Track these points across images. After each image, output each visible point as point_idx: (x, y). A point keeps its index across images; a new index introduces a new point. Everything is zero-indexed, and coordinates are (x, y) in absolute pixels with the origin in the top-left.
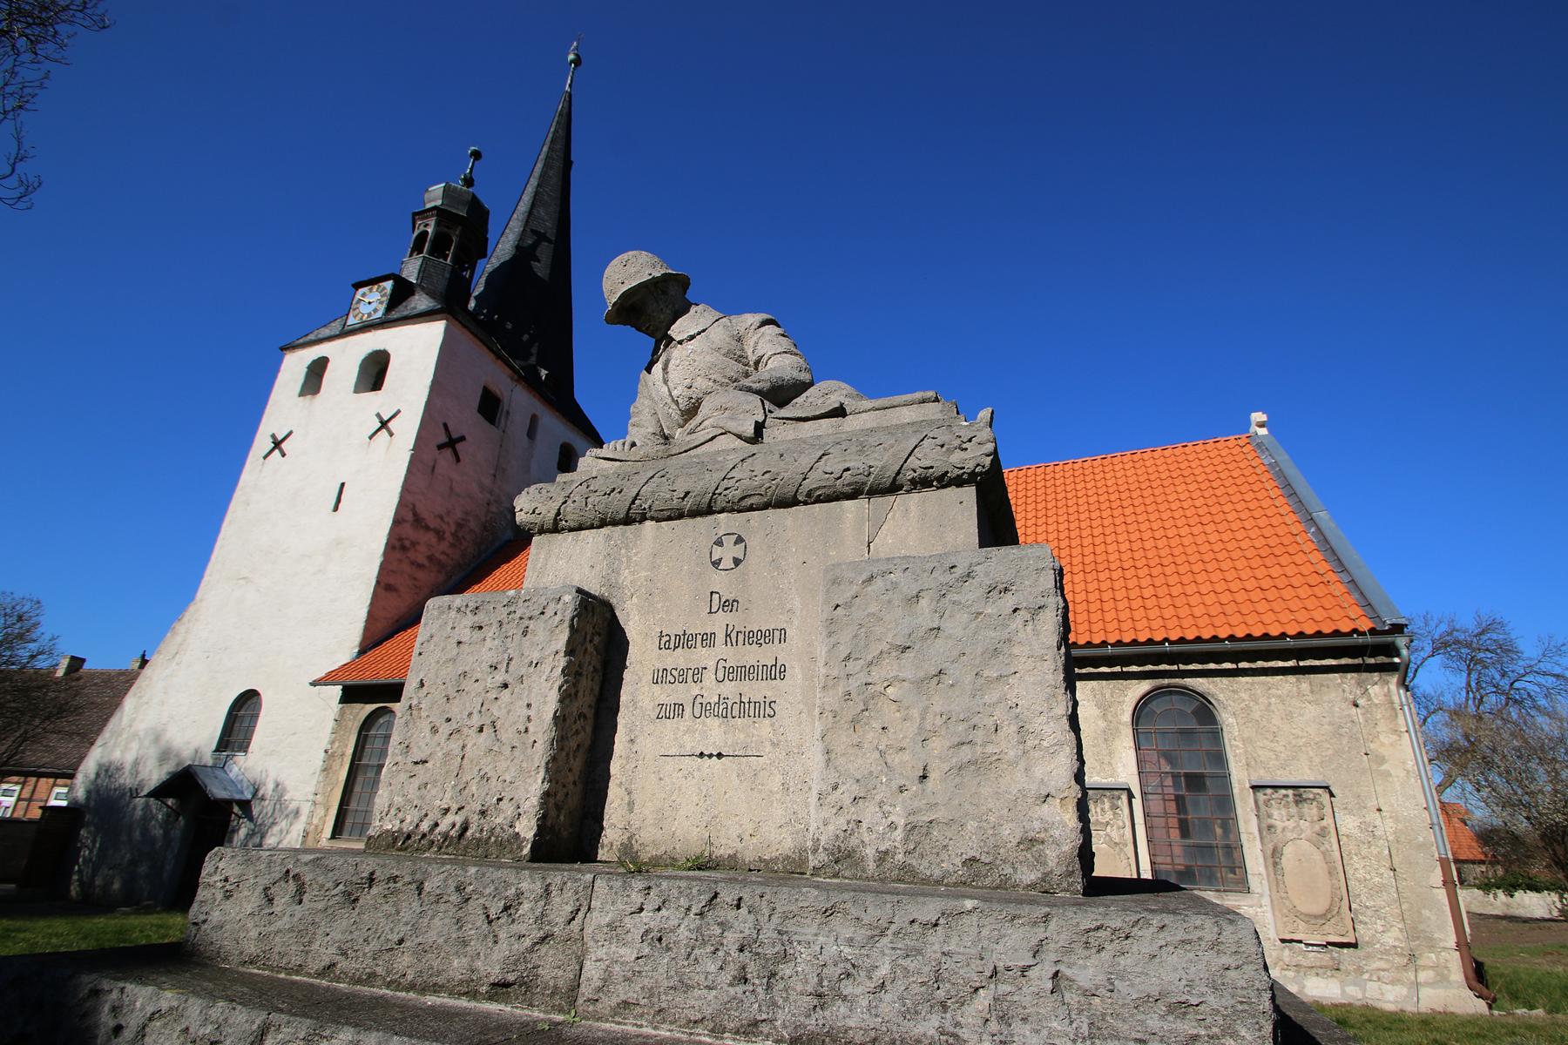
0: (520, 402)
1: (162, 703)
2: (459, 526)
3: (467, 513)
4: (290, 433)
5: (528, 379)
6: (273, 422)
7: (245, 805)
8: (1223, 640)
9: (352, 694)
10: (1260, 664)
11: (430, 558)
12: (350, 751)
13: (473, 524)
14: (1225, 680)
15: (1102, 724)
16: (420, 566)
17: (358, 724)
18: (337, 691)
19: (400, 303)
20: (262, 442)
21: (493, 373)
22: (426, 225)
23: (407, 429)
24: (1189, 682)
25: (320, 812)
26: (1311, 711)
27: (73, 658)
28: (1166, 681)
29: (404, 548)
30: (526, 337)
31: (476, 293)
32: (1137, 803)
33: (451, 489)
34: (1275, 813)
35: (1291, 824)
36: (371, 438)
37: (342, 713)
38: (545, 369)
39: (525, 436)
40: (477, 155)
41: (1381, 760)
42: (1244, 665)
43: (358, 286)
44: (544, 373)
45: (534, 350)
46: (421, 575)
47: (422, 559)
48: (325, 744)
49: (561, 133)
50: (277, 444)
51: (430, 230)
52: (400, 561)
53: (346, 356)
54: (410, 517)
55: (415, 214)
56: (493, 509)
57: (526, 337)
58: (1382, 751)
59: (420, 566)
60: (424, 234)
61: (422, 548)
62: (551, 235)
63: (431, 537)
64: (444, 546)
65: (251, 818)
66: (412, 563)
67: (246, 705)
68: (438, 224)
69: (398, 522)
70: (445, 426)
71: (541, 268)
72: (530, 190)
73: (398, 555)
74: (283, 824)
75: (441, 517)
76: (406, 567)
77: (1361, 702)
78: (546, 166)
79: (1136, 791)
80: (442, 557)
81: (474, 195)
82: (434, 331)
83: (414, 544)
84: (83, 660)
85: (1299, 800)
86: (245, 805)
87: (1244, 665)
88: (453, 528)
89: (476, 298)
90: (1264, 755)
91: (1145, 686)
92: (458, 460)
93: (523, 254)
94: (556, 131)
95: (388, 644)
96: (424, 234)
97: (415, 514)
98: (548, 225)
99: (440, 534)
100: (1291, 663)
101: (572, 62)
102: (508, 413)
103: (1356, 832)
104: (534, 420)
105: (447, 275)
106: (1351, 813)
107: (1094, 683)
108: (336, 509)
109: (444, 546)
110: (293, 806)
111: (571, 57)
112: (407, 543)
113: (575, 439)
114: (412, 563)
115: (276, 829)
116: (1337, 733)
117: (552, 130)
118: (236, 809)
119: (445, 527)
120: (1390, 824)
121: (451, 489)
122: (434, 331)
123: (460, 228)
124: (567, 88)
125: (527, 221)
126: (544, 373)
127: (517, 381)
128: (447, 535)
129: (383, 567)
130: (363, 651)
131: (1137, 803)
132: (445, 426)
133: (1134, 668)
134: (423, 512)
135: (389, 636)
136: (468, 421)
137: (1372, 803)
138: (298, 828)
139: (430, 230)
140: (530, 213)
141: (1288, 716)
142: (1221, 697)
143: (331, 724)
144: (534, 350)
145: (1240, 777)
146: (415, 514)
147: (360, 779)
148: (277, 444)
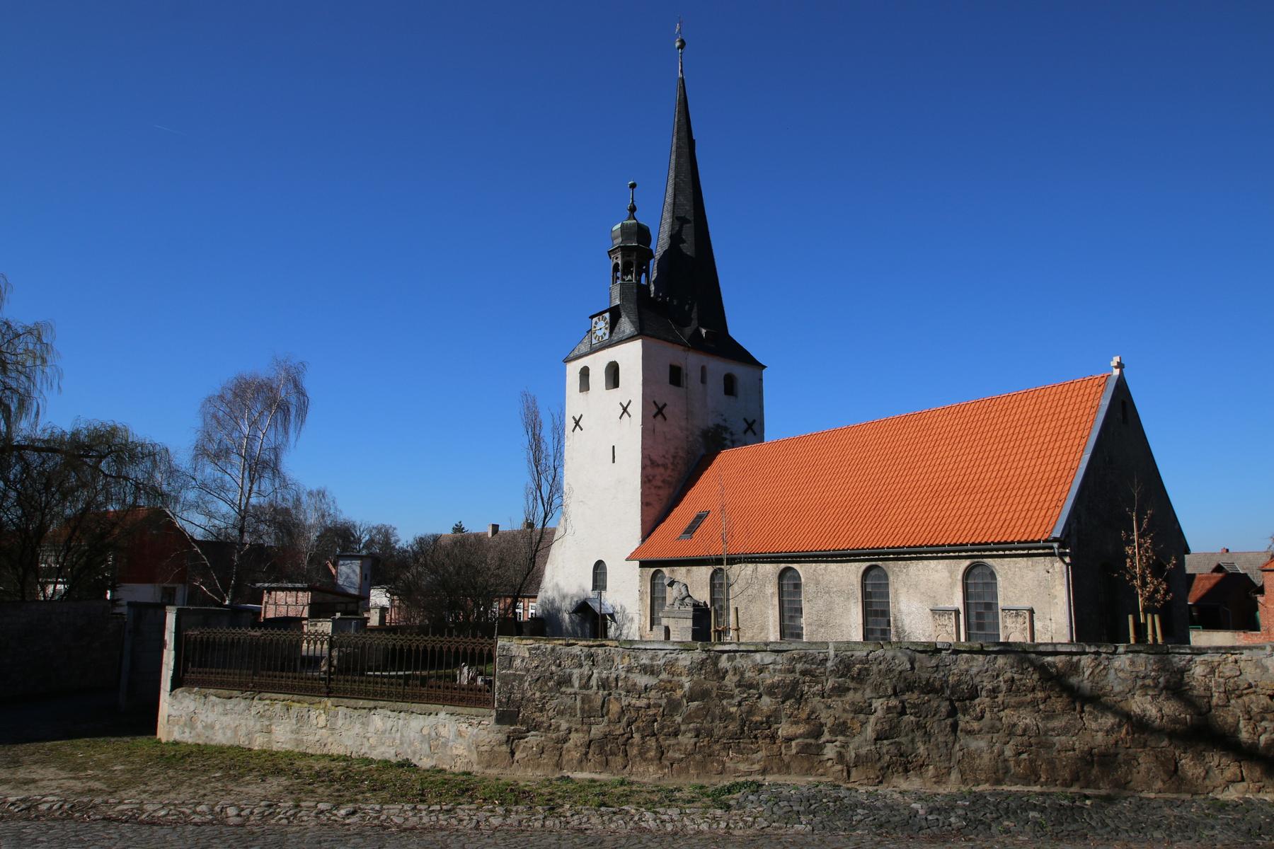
0: (692, 361)
1: (564, 567)
2: (674, 457)
3: (677, 448)
4: (581, 416)
5: (696, 344)
6: (571, 411)
7: (612, 615)
8: (990, 544)
9: (643, 564)
10: (1014, 552)
11: (663, 481)
12: (649, 591)
13: (681, 454)
14: (999, 560)
15: (950, 580)
16: (659, 487)
17: (649, 578)
18: (637, 563)
19: (615, 325)
20: (570, 424)
21: (672, 354)
22: (617, 258)
23: (636, 410)
24: (985, 560)
25: (643, 619)
26: (1031, 574)
27: (493, 525)
28: (976, 560)
29: (650, 481)
30: (687, 307)
31: (653, 279)
32: (962, 616)
33: (665, 438)
34: (1008, 621)
35: (1013, 625)
36: (620, 418)
37: (642, 572)
38: (705, 328)
39: (699, 383)
40: (633, 186)
41: (1055, 597)
42: (1007, 552)
43: (592, 317)
44: (704, 331)
45: (694, 315)
46: (661, 492)
47: (659, 484)
48: (638, 588)
49: (683, 120)
50: (577, 423)
51: (620, 262)
52: (649, 488)
53: (597, 363)
54: (649, 463)
55: (609, 252)
56: (691, 439)
57: (687, 307)
58: (1056, 593)
59: (659, 487)
60: (617, 265)
61: (658, 477)
62: (690, 217)
63: (661, 470)
64: (669, 472)
65: (616, 622)
66: (655, 487)
67: (599, 568)
68: (623, 257)
69: (644, 468)
70: (655, 402)
71: (688, 248)
72: (671, 182)
73: (648, 485)
74: (629, 625)
75: (664, 456)
76: (653, 491)
77: (1050, 570)
78: (678, 157)
79: (962, 611)
80: (669, 479)
81: (639, 225)
82: (637, 346)
83: (654, 477)
84: (498, 526)
85: (1017, 615)
86: (612, 615)
87: (1007, 552)
88: (671, 460)
89: (654, 282)
90: (1010, 594)
91: (967, 562)
92: (665, 419)
93: (675, 238)
94: (679, 120)
95: (654, 534)
96: (617, 265)
97: (651, 460)
98: (689, 214)
99: (665, 466)
100: (1026, 552)
101: (678, 48)
102: (687, 374)
103: (1041, 629)
104: (703, 369)
105: (635, 291)
106: (1040, 621)
107: (947, 561)
108: (614, 462)
109: (669, 472)
110: (630, 617)
111: (678, 44)
112: (651, 478)
113: (738, 370)
114: (655, 487)
115: (625, 627)
116: (1040, 586)
117: (676, 120)
118: (608, 617)
119: (667, 461)
120: (1054, 625)
121: (665, 438)
122: (637, 346)
123: (635, 254)
124: (680, 75)
125: (674, 212)
126: (704, 331)
127: (689, 350)
128: (669, 465)
129: (642, 494)
130: (643, 541)
131: (962, 616)
132: (655, 402)
133: (964, 554)
134: (654, 457)
135: (653, 530)
136: (667, 393)
137: (1048, 617)
138: (635, 626)
139: (620, 262)
140: (674, 203)
141: (1022, 577)
142: (997, 568)
143: (638, 578)
144: (694, 315)
145: (1001, 604)
146: (651, 460)
147: (656, 603)
148: (577, 423)
